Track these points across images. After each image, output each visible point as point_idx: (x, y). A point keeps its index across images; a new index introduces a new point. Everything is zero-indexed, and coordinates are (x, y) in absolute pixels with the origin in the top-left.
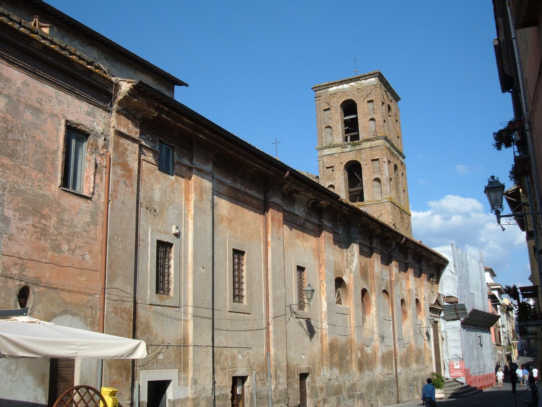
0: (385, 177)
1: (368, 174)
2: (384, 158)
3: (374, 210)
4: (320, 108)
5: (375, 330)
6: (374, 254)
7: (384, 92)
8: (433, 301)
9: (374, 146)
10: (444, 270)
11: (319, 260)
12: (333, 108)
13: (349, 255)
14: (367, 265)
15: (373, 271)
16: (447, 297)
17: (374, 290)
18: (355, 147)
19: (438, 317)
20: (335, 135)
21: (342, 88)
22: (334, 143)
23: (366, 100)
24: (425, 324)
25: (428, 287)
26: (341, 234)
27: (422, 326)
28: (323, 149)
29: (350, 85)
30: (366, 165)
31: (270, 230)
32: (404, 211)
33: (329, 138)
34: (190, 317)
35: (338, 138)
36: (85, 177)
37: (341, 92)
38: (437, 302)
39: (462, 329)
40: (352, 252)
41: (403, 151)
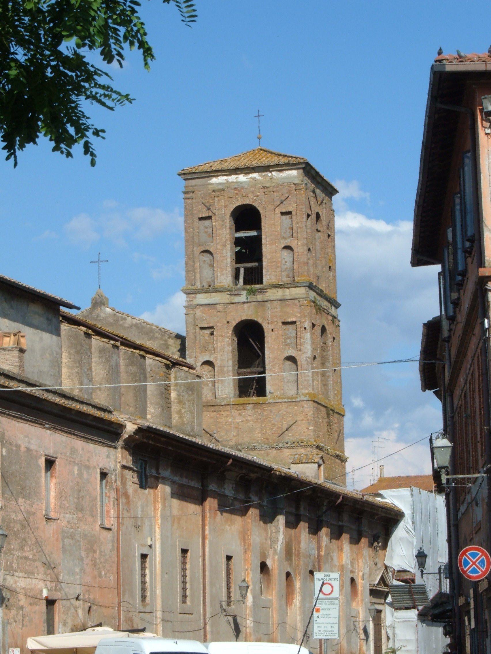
1: (276, 347)
2: (305, 321)
3: (284, 413)
4: (192, 214)
5: (298, 627)
7: (312, 194)
8: (376, 579)
9: (288, 298)
10: (396, 528)
11: (245, 545)
12: (217, 219)
13: (274, 531)
14: (291, 540)
15: (299, 547)
16: (398, 571)
17: (300, 574)
18: (254, 295)
19: (383, 604)
20: (219, 270)
21: (235, 181)
23: (278, 211)
24: (361, 617)
25: (369, 557)
26: (266, 506)
27: (358, 619)
28: (196, 294)
29: (251, 178)
30: (272, 330)
31: (207, 522)
33: (207, 273)
34: (159, 620)
35: (223, 274)
36: (106, 511)
37: (233, 187)
38: (383, 580)
39: (420, 623)
40: (277, 527)
41: (336, 293)
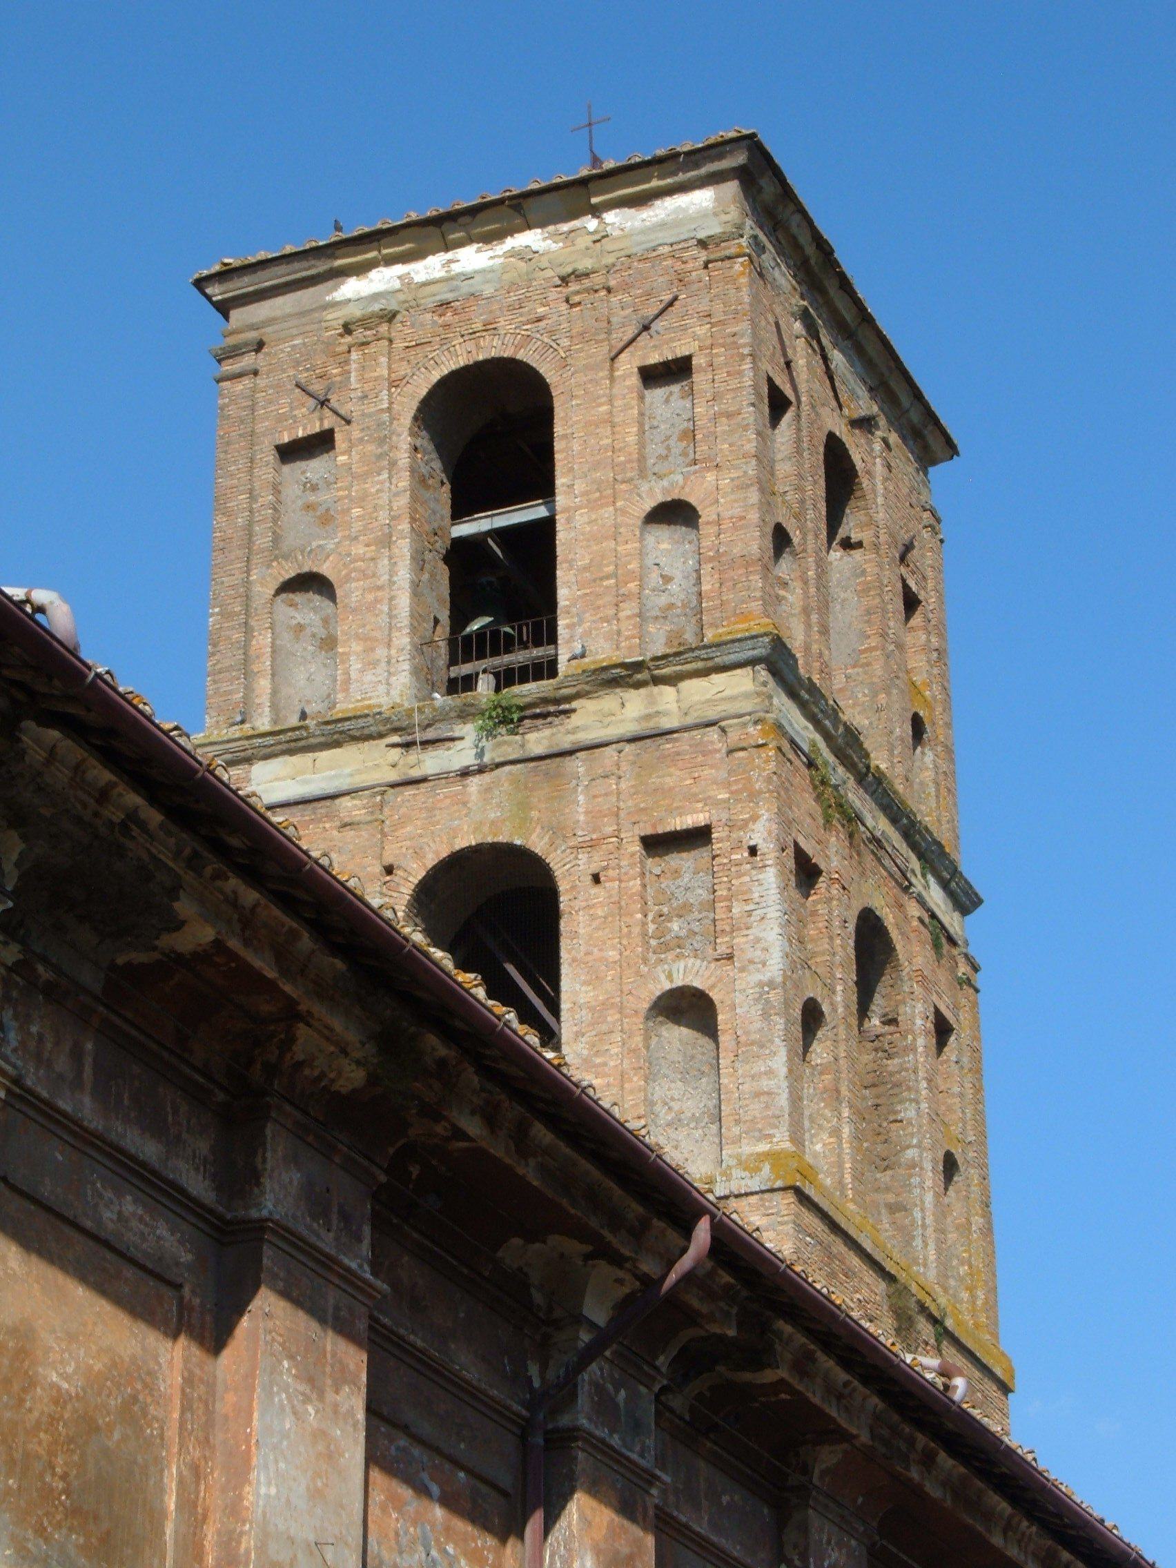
0: (755, 977)
2: (755, 818)
6: (266, 1302)
7: (798, 326)
15: (235, 1510)
18: (513, 732)
20: (356, 647)
21: (439, 274)
22: (344, 706)
23: (629, 365)
28: (248, 760)
29: (512, 254)
30: (596, 879)
32: (935, 1321)
35: (374, 664)
37: (430, 302)
